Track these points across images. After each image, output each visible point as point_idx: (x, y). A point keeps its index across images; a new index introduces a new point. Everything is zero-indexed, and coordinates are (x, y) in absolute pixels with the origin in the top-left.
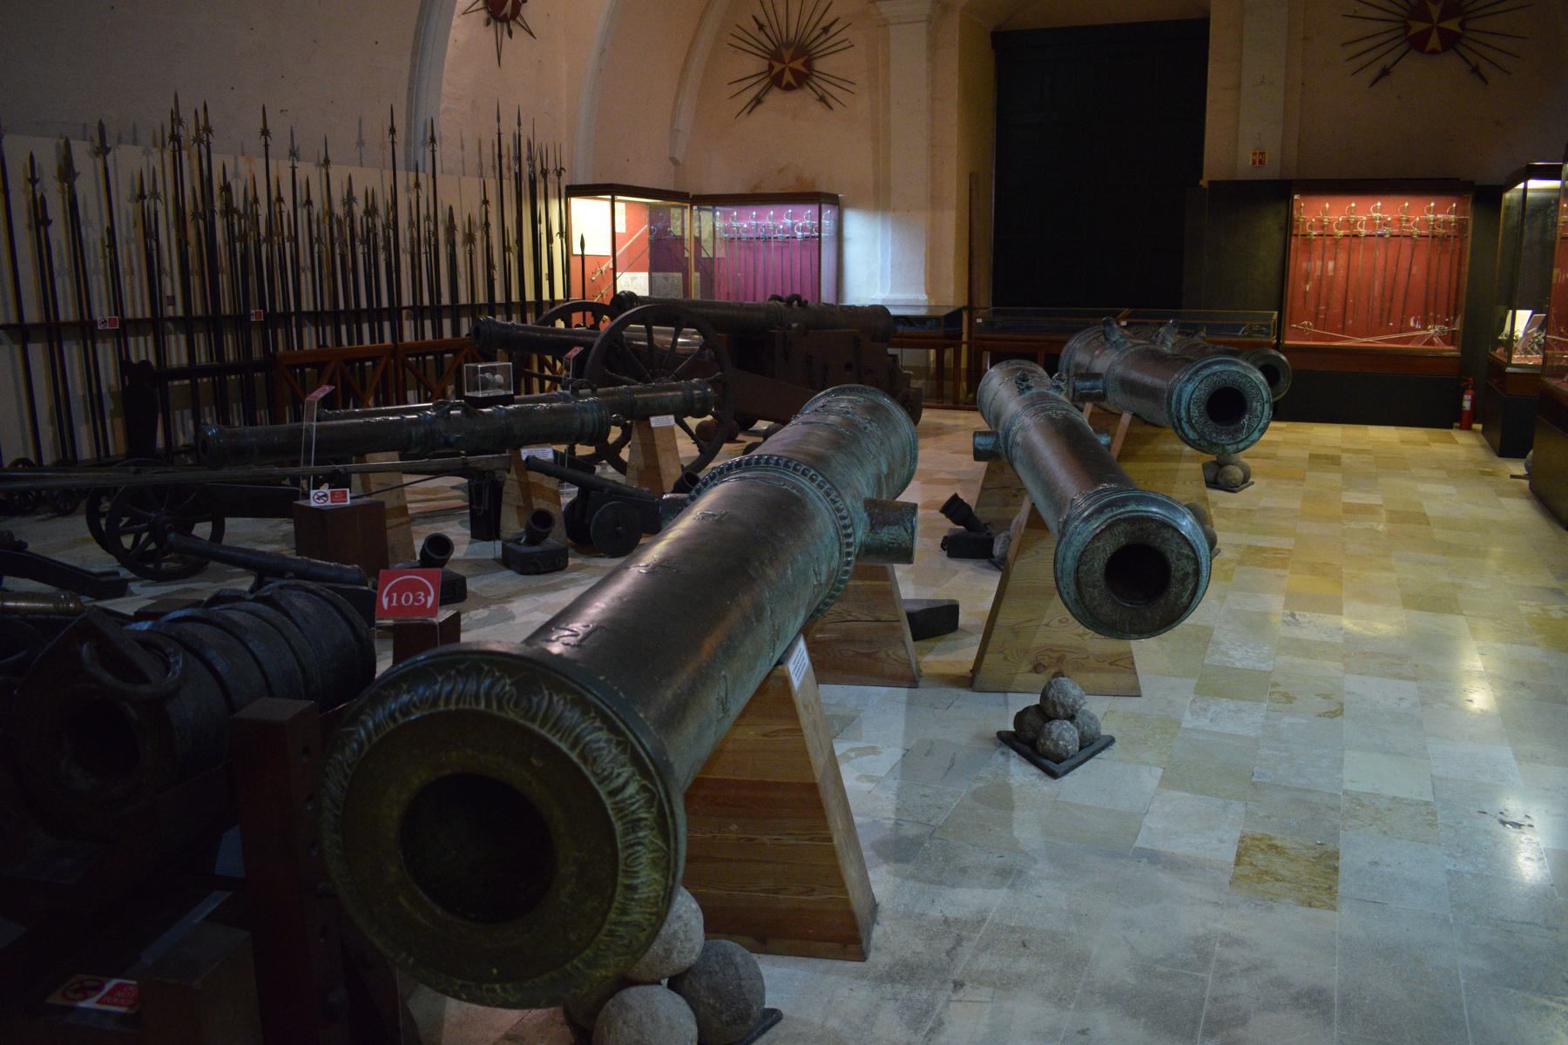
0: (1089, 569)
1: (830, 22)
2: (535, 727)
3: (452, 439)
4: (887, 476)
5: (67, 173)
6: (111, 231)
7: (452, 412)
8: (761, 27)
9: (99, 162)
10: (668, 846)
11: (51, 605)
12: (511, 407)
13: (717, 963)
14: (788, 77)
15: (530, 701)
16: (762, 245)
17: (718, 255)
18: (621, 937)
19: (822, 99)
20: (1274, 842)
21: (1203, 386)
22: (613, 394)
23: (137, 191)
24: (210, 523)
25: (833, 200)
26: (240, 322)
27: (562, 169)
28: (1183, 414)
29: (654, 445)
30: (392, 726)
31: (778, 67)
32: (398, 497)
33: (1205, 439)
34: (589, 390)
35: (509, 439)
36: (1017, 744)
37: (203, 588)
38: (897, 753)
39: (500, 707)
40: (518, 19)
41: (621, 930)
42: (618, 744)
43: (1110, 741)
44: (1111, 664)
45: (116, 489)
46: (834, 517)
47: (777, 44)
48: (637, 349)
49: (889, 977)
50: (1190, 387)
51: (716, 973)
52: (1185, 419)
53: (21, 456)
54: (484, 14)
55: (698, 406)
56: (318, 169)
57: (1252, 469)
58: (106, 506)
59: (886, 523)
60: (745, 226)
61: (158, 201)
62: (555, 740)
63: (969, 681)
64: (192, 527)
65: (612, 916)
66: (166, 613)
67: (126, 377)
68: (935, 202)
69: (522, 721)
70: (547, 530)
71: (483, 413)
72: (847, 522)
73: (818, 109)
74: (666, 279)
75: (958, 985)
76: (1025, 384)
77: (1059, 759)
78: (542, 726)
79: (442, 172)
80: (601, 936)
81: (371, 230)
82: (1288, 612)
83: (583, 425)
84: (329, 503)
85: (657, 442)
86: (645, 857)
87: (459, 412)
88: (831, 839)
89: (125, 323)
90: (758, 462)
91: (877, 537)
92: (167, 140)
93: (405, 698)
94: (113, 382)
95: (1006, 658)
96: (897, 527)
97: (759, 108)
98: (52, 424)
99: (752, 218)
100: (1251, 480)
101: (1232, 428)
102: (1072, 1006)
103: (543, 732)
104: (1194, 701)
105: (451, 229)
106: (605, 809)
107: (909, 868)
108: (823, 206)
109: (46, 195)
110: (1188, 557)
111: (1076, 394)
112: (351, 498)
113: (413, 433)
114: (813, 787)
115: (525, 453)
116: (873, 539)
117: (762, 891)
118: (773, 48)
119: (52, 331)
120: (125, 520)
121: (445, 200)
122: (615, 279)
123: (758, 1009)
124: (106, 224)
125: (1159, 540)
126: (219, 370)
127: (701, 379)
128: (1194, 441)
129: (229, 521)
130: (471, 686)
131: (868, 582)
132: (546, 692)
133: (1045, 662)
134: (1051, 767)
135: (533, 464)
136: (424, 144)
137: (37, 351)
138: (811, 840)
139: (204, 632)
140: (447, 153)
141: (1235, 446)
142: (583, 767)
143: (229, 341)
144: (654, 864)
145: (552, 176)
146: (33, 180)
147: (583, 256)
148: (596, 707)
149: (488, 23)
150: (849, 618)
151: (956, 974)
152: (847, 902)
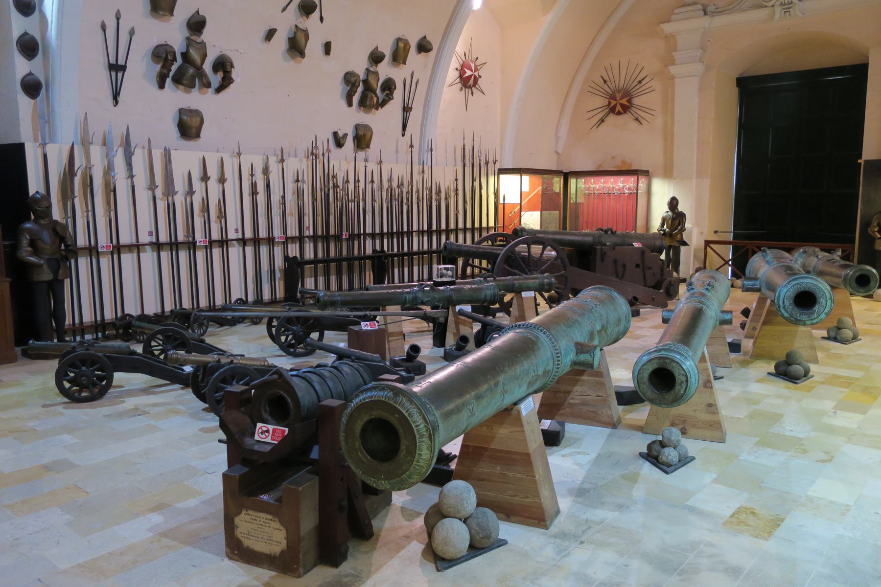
0: (642, 377)
1: (642, 78)
2: (397, 406)
3: (424, 301)
4: (599, 332)
5: (266, 171)
6: (284, 197)
7: (425, 289)
8: (605, 82)
9: (280, 165)
10: (432, 444)
11: (200, 380)
12: (452, 287)
13: (481, 514)
14: (619, 108)
15: (396, 399)
16: (607, 198)
17: (578, 201)
18: (417, 470)
19: (637, 119)
20: (755, 511)
21: (791, 290)
22: (504, 280)
23: (296, 178)
24: (318, 333)
25: (646, 173)
26: (338, 238)
27: (496, 160)
28: (781, 304)
29: (523, 306)
30: (360, 403)
31: (613, 103)
32: (399, 326)
33: (793, 317)
34: (492, 278)
35: (449, 302)
36: (649, 458)
37: (313, 361)
38: (593, 455)
39: (388, 400)
40: (477, 86)
41: (417, 467)
42: (419, 413)
43: (693, 459)
44: (710, 426)
45: (280, 317)
46: (552, 350)
47: (613, 90)
48: (523, 258)
49: (556, 536)
50: (785, 290)
51: (480, 518)
52: (782, 306)
53: (240, 297)
54: (460, 85)
55: (547, 287)
56: (377, 166)
57: (860, 331)
58: (275, 323)
59: (583, 352)
60: (597, 187)
61: (304, 184)
62: (402, 410)
63: (641, 429)
64: (310, 334)
65: (415, 462)
66: (301, 370)
67: (286, 263)
68: (700, 174)
69: (394, 404)
70: (466, 344)
71: (439, 289)
72: (558, 351)
73: (634, 125)
74: (550, 214)
75: (582, 543)
76: (690, 287)
77: (669, 466)
78: (399, 406)
79: (436, 165)
80: (411, 468)
81: (401, 194)
82: (833, 411)
83: (486, 295)
84: (369, 328)
85: (524, 304)
86: (425, 447)
87: (428, 288)
88: (535, 477)
89: (287, 238)
90: (527, 325)
91: (579, 358)
92: (310, 155)
93: (364, 396)
94: (280, 264)
95: (658, 419)
96: (587, 354)
97: (603, 124)
98: (253, 283)
99: (601, 183)
100: (859, 338)
101: (808, 312)
102: (625, 556)
103: (399, 407)
104: (752, 448)
105: (439, 192)
106: (414, 431)
107: (580, 500)
108: (639, 177)
109: (257, 182)
110: (683, 375)
111: (744, 288)
112: (378, 326)
113: (408, 297)
114: (528, 455)
115: (458, 308)
116: (577, 359)
117: (508, 495)
118: (611, 92)
119: (256, 241)
120: (283, 329)
121: (437, 178)
122: (520, 216)
123: (495, 535)
124: (282, 194)
125: (671, 367)
126: (327, 261)
127: (550, 275)
128: (787, 318)
129: (326, 332)
130: (382, 393)
131: (594, 378)
132: (401, 397)
133: (677, 422)
134: (666, 469)
135: (461, 313)
136: (428, 150)
137: (249, 250)
138: (527, 476)
139: (314, 377)
140: (438, 154)
141: (811, 321)
142: (409, 418)
143: (332, 246)
144: (428, 448)
145: (491, 164)
146: (252, 175)
147: (504, 204)
148: (414, 402)
149: (461, 89)
150: (585, 394)
151: (583, 539)
152: (541, 504)
